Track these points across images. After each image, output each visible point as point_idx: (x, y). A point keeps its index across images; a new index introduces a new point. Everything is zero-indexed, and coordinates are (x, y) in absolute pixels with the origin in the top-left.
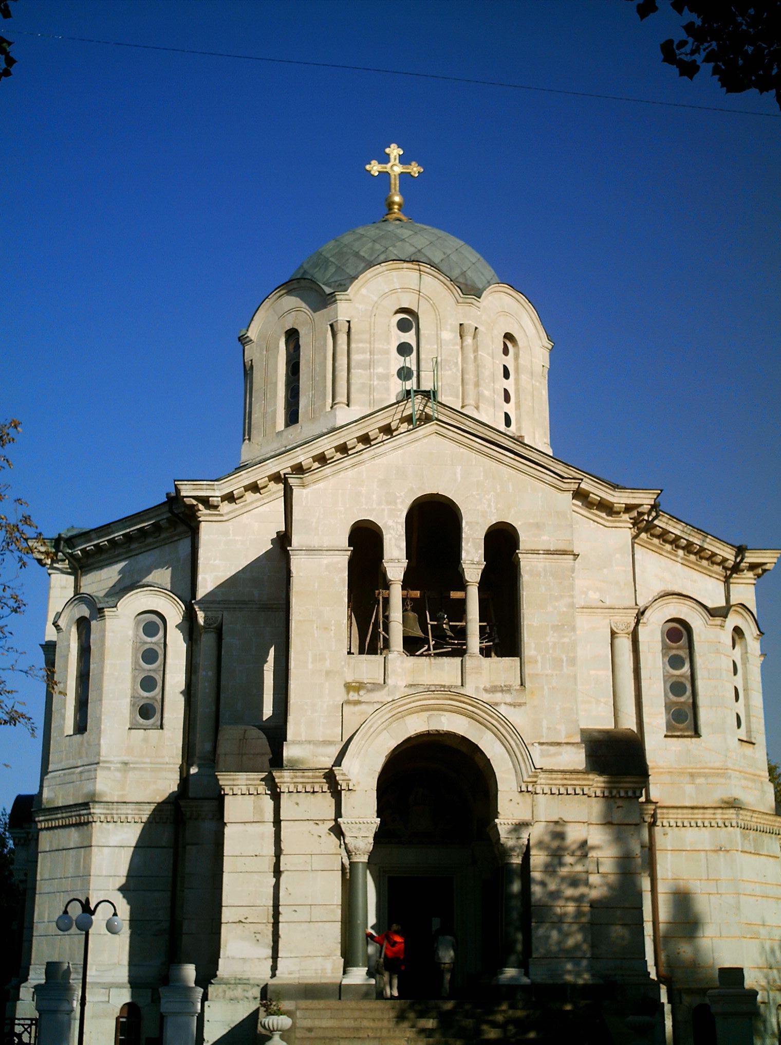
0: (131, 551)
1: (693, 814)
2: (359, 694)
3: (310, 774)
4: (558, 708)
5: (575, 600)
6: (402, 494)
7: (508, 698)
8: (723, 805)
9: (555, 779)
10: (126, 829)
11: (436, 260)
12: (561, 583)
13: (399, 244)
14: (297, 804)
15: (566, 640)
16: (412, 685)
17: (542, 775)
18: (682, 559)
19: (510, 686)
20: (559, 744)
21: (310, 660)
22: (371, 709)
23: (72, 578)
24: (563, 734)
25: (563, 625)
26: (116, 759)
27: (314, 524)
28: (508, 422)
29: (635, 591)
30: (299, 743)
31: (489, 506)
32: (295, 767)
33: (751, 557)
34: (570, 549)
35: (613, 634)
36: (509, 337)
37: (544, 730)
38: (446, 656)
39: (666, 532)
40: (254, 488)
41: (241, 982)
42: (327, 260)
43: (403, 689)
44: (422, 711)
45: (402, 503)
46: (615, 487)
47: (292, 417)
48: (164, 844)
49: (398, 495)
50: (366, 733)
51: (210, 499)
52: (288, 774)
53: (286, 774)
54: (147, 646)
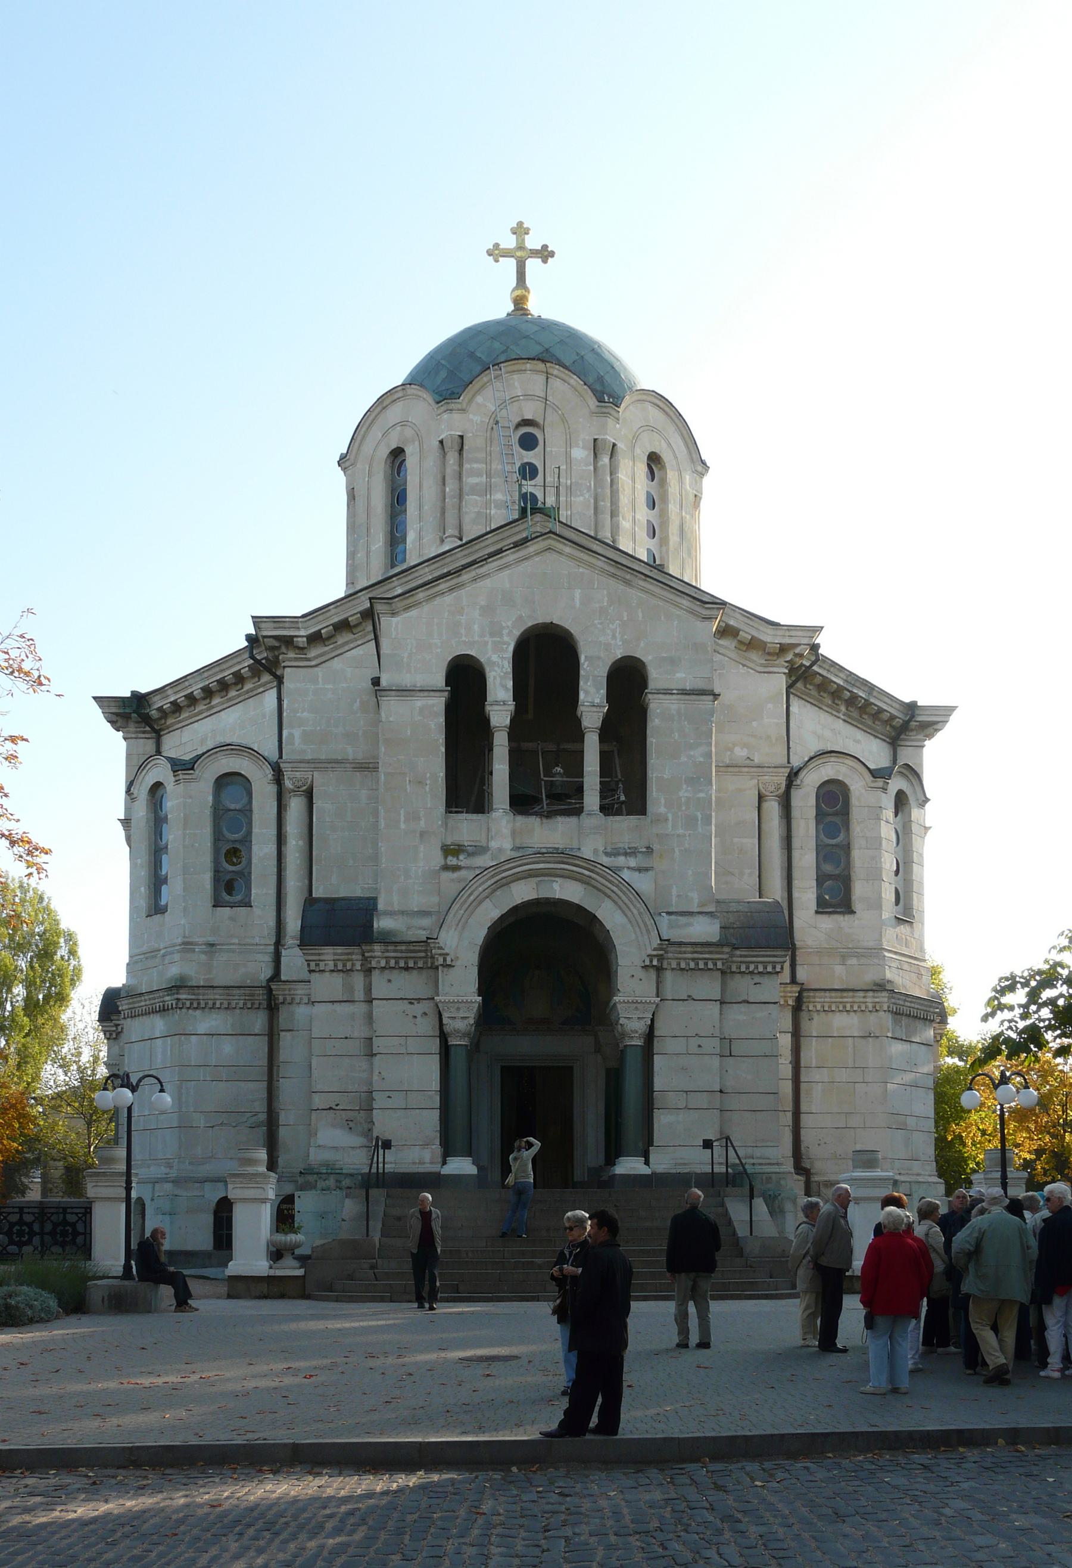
0: (213, 707)
2: (458, 859)
3: (403, 948)
4: (690, 872)
6: (509, 623)
7: (632, 862)
8: (874, 988)
9: (685, 953)
10: (214, 1016)
12: (698, 728)
14: (389, 981)
15: (702, 795)
16: (519, 848)
19: (636, 848)
20: (691, 914)
21: (402, 818)
26: (201, 940)
27: (405, 660)
29: (789, 748)
31: (614, 637)
32: (387, 939)
34: (709, 688)
35: (761, 798)
38: (560, 815)
41: (333, 1171)
43: (509, 852)
44: (530, 876)
45: (509, 634)
48: (257, 1031)
49: (504, 624)
50: (465, 901)
51: (295, 639)
52: (379, 948)
53: (377, 947)
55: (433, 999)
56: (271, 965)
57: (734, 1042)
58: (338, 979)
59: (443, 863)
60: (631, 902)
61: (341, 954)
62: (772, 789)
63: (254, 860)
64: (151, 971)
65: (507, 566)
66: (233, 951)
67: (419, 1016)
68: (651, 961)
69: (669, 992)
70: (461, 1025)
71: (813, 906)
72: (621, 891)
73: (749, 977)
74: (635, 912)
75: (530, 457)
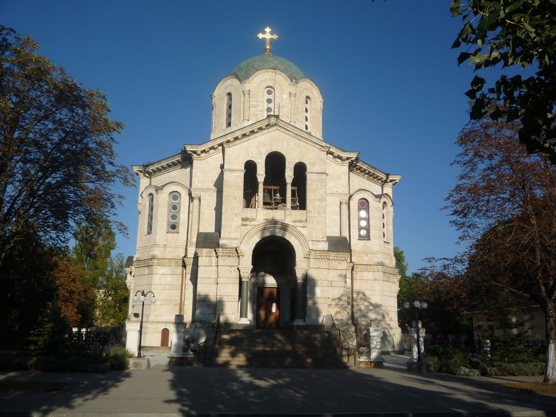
1: (367, 267)
3: (229, 250)
4: (319, 228)
7: (301, 224)
9: (317, 253)
10: (165, 268)
11: (282, 69)
12: (321, 184)
13: (268, 63)
14: (224, 260)
15: (323, 204)
17: (312, 252)
18: (367, 177)
19: (302, 220)
20: (319, 241)
23: (149, 179)
24: (321, 237)
25: (322, 199)
29: (349, 188)
30: (225, 239)
31: (296, 156)
32: (224, 247)
33: (391, 178)
34: (325, 172)
35: (341, 203)
36: (308, 97)
37: (314, 236)
39: (361, 168)
40: (212, 148)
45: (264, 154)
46: (344, 151)
47: (229, 124)
48: (178, 274)
50: (248, 236)
53: (220, 249)
54: (174, 204)
56: (185, 252)
57: (332, 282)
58: (207, 258)
59: (242, 223)
61: (209, 251)
62: (344, 201)
65: (264, 134)
68: (307, 256)
69: (312, 265)
71: (358, 238)
72: (297, 233)
73: (337, 261)
74: (302, 240)
75: (271, 97)
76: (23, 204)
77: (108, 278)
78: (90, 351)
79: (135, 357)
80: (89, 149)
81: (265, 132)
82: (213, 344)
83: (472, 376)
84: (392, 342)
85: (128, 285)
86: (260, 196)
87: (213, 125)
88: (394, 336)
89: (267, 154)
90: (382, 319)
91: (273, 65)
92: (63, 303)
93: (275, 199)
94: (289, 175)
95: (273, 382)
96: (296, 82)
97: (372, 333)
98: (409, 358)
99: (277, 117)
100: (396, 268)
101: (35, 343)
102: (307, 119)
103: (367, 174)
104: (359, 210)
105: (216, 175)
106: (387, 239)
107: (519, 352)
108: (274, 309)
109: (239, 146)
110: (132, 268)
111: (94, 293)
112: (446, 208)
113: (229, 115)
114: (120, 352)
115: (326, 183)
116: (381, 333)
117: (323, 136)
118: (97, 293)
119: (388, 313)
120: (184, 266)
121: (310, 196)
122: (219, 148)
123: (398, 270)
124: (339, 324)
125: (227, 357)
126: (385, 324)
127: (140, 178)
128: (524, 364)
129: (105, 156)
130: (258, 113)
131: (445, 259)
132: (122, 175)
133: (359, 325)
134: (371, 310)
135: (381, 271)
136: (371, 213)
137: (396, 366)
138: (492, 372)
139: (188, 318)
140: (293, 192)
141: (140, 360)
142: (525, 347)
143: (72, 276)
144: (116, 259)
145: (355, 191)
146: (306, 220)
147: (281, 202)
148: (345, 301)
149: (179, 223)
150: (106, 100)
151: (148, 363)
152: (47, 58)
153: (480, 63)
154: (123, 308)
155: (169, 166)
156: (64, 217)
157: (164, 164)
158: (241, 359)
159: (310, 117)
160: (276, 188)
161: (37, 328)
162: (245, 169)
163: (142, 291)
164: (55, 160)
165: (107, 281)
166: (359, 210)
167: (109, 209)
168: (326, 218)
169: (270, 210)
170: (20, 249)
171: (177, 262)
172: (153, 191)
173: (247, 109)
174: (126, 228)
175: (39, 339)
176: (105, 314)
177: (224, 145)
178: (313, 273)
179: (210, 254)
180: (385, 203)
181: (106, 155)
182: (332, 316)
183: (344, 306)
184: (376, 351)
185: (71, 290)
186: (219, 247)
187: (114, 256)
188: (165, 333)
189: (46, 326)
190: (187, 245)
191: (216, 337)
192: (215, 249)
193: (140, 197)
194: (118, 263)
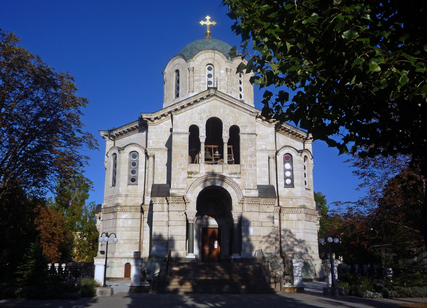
1: (292, 210)
3: (177, 198)
4: (250, 179)
5: (257, 148)
6: (205, 117)
7: (236, 176)
8: (300, 207)
9: (249, 199)
10: (127, 214)
11: (220, 50)
14: (174, 206)
15: (253, 159)
17: (245, 198)
18: (290, 136)
19: (237, 173)
20: (251, 189)
21: (178, 165)
22: (195, 179)
24: (252, 186)
25: (252, 155)
28: (241, 96)
30: (175, 189)
31: (231, 120)
32: (173, 196)
35: (269, 158)
39: (285, 128)
40: (163, 115)
42: (187, 50)
43: (204, 174)
45: (205, 119)
47: (177, 96)
48: (138, 218)
50: (193, 186)
53: (171, 198)
54: (133, 161)
55: (185, 211)
58: (160, 206)
59: (188, 176)
60: (236, 186)
61: (161, 199)
62: (272, 156)
63: (139, 173)
64: (110, 201)
66: (132, 196)
67: (181, 215)
68: (241, 201)
70: (192, 218)
71: (284, 186)
72: (233, 184)
73: (266, 205)
74: (237, 189)
75: (211, 72)
76: (9, 166)
77: (83, 223)
78: (65, 282)
79: (101, 286)
80: (61, 121)
81: (205, 101)
82: (165, 275)
83: (376, 298)
84: (314, 271)
85: (98, 228)
86: (202, 154)
87: (165, 96)
88: (316, 266)
89: (210, 117)
90: (306, 252)
91: (212, 46)
92: (47, 244)
93: (214, 156)
94: (226, 136)
95: (211, 305)
96: (231, 60)
97: (295, 263)
98: (326, 283)
99: (215, 89)
100: (317, 210)
101: (21, 276)
102: (241, 90)
103: (291, 133)
104: (285, 163)
105: (167, 137)
106: (308, 186)
107: (416, 278)
108: (216, 246)
109: (184, 113)
110: (100, 214)
111: (72, 235)
112: (349, 161)
113: (178, 88)
114: (90, 283)
115: (256, 141)
116: (302, 264)
117: (255, 103)
118: (74, 235)
119: (310, 247)
120: (142, 211)
121: (243, 153)
122: (168, 115)
123: (318, 212)
124: (268, 257)
125: (176, 285)
126: (308, 256)
127: (106, 141)
128: (419, 287)
129: (74, 125)
130: (201, 85)
131: (349, 202)
132: (87, 140)
133: (286, 258)
134: (296, 245)
135: (303, 213)
136: (294, 165)
137: (316, 291)
138: (393, 294)
139: (145, 254)
140: (229, 150)
141: (105, 289)
142: (422, 273)
143: (54, 221)
144: (89, 207)
145: (281, 148)
146: (240, 173)
147: (219, 158)
148: (274, 238)
149: (137, 177)
150: (74, 81)
151: (111, 291)
152: (26, 50)
153: (262, 84)
154: (95, 247)
155: (129, 130)
156: (44, 175)
157: (125, 129)
158: (187, 287)
159: (244, 88)
160: (215, 146)
161: (23, 264)
162: (189, 132)
163: (106, 233)
164: (34, 130)
165: (82, 225)
166: (285, 163)
167: (78, 167)
168: (256, 170)
169: (210, 165)
170: (8, 200)
171: (137, 208)
172: (116, 151)
173: (192, 83)
174: (92, 182)
175: (24, 273)
176: (81, 251)
177: (172, 113)
178: (246, 215)
179: (162, 202)
180: (306, 156)
181: (74, 125)
182: (262, 251)
183: (273, 242)
184: (298, 279)
185: (53, 233)
186: (169, 196)
187: (88, 204)
188: (128, 267)
189: (30, 263)
190: (144, 195)
191: (167, 269)
192: (166, 197)
193: (106, 156)
194: (91, 210)
